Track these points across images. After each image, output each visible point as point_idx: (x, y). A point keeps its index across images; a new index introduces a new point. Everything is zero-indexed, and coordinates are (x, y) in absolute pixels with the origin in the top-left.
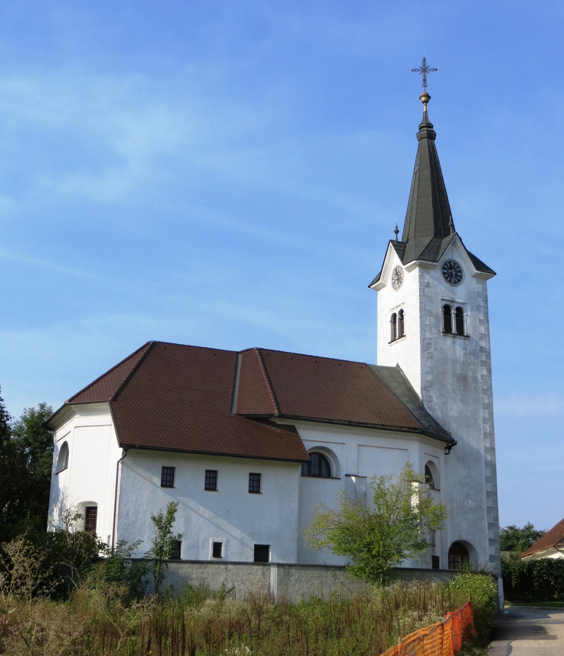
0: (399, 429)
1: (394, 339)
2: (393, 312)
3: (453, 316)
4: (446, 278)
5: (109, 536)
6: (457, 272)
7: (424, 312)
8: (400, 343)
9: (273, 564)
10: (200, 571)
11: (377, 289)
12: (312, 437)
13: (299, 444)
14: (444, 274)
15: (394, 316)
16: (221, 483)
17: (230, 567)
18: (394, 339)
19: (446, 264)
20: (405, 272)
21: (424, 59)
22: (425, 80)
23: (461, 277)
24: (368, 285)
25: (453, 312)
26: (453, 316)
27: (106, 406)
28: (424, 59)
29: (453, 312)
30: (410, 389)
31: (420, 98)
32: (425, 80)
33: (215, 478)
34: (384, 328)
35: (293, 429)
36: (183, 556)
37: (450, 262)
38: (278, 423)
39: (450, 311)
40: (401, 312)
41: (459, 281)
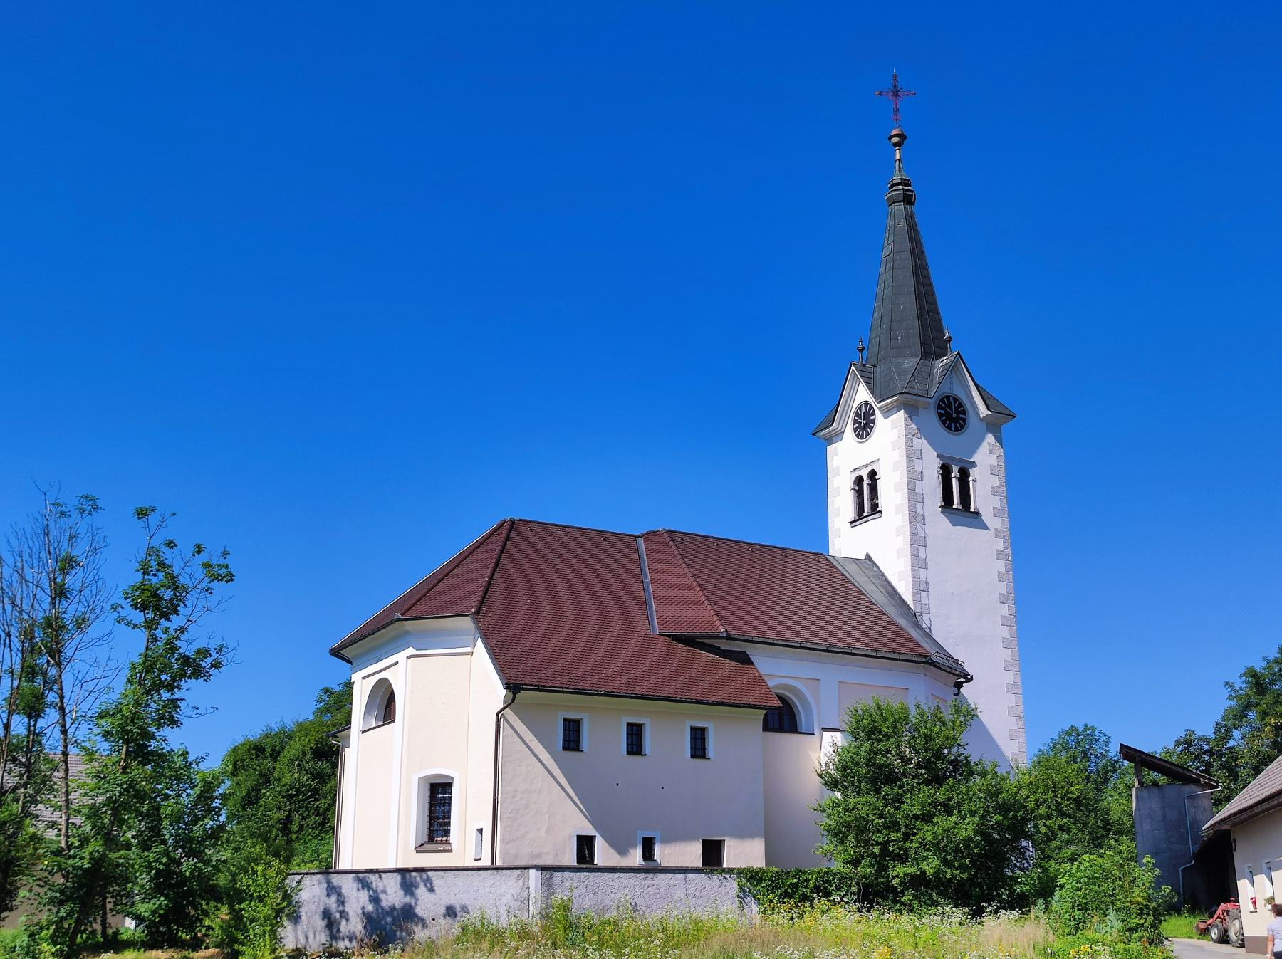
0: (896, 656)
1: (860, 516)
2: (856, 474)
3: (955, 483)
4: (943, 422)
5: (480, 831)
6: (958, 413)
7: (914, 477)
8: (870, 527)
9: (729, 871)
10: (647, 882)
11: (830, 440)
12: (777, 670)
13: (759, 681)
14: (940, 415)
15: (859, 480)
16: (649, 741)
17: (690, 876)
18: (860, 516)
19: (942, 400)
20: (879, 416)
21: (895, 76)
22: (896, 110)
23: (964, 420)
24: (812, 430)
25: (955, 474)
26: (955, 483)
27: (467, 623)
28: (895, 76)
29: (955, 474)
30: (893, 594)
31: (890, 138)
32: (896, 110)
33: (703, 739)
34: (841, 501)
35: (744, 659)
36: (598, 860)
37: (948, 397)
38: (723, 648)
39: (950, 473)
40: (873, 474)
41: (962, 427)
